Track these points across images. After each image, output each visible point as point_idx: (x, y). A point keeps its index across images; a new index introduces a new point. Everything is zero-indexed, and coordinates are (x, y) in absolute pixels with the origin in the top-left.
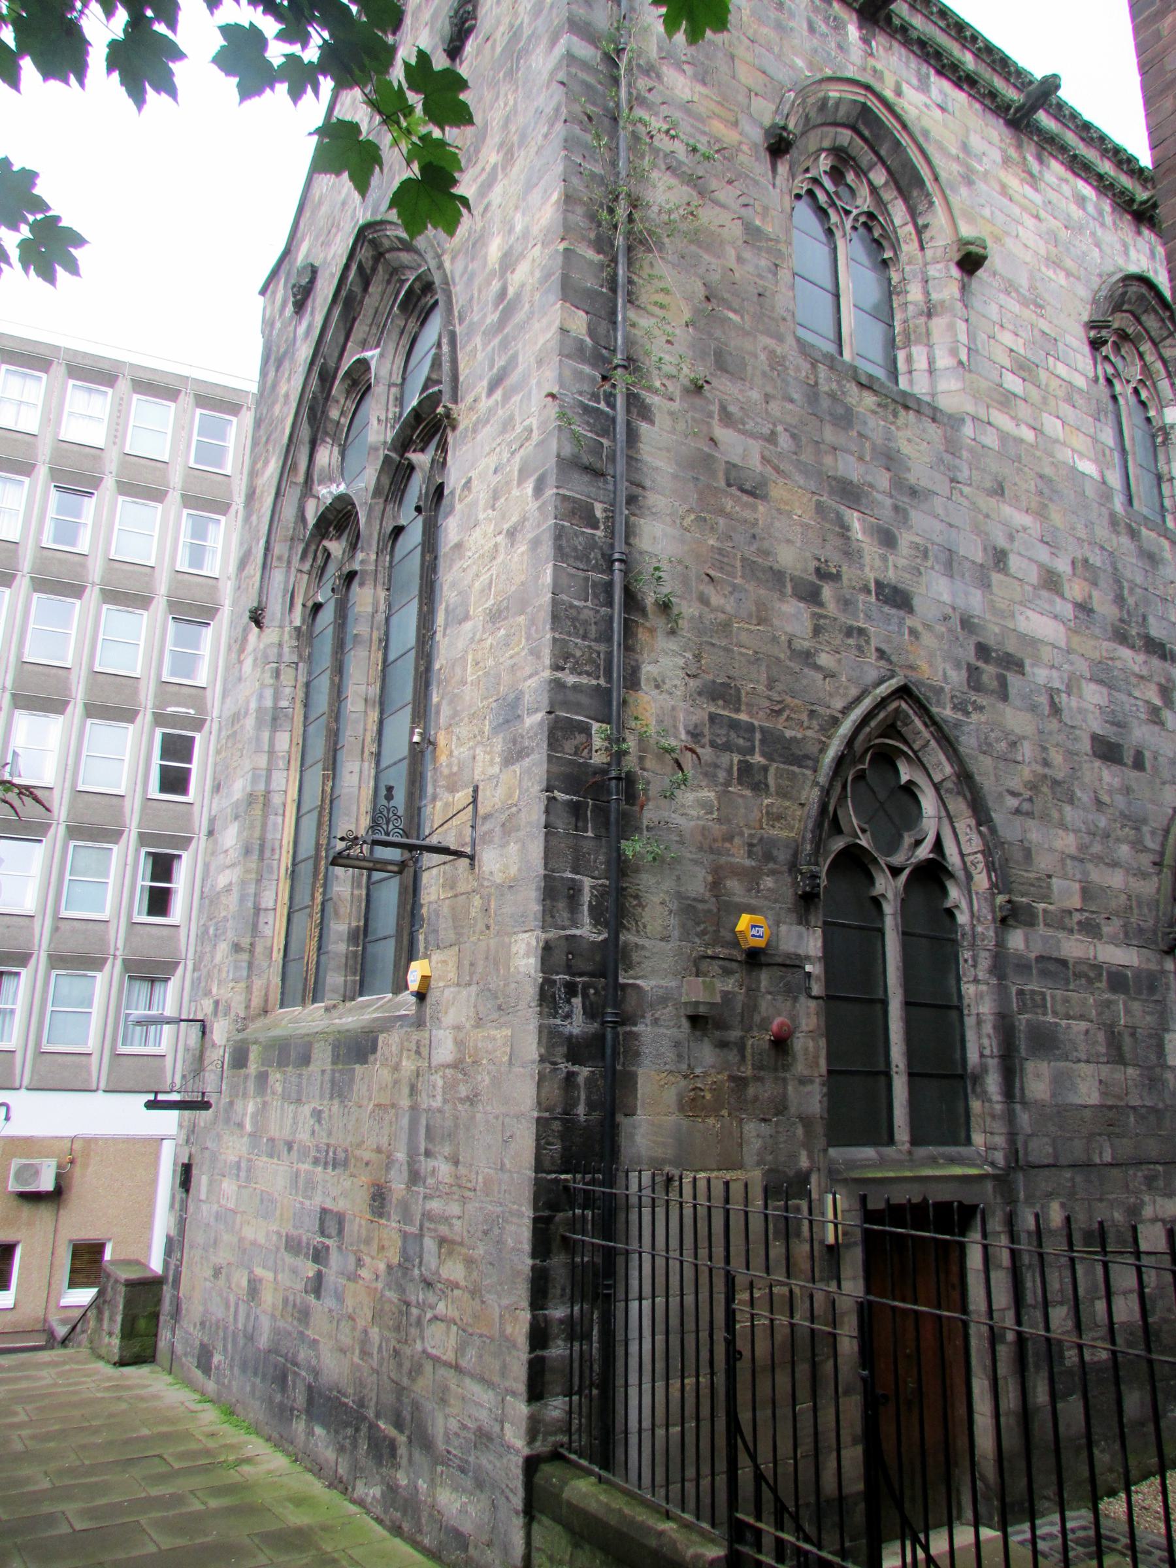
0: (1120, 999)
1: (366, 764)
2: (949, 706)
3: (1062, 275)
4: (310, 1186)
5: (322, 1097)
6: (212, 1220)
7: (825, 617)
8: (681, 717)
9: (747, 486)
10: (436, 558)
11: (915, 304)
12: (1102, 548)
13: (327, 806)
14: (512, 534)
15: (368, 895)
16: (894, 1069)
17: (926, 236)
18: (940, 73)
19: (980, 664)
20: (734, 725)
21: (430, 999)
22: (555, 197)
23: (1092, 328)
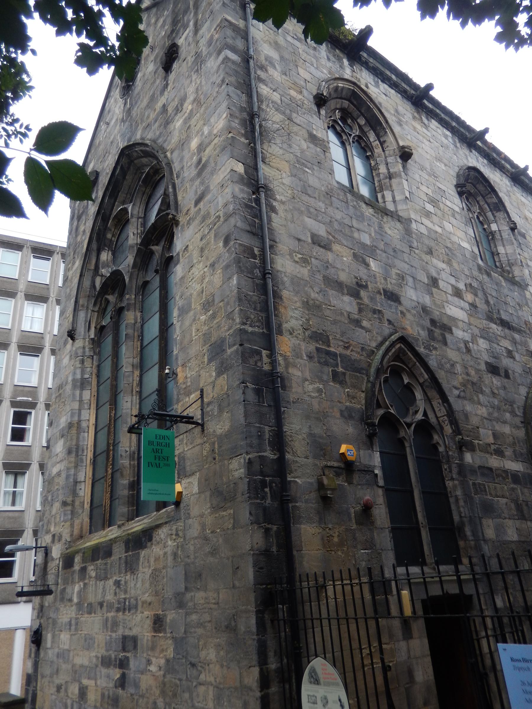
0: (518, 487)
1: (134, 397)
2: (422, 347)
3: (443, 165)
4: (115, 624)
5: (120, 573)
6: (55, 658)
7: (363, 304)
8: (303, 348)
9: (322, 244)
10: (167, 292)
12: (476, 279)
16: (421, 525)
17: (385, 145)
18: (383, 81)
19: (433, 328)
20: (328, 353)
21: (182, 505)
22: (225, 115)
23: (458, 187)
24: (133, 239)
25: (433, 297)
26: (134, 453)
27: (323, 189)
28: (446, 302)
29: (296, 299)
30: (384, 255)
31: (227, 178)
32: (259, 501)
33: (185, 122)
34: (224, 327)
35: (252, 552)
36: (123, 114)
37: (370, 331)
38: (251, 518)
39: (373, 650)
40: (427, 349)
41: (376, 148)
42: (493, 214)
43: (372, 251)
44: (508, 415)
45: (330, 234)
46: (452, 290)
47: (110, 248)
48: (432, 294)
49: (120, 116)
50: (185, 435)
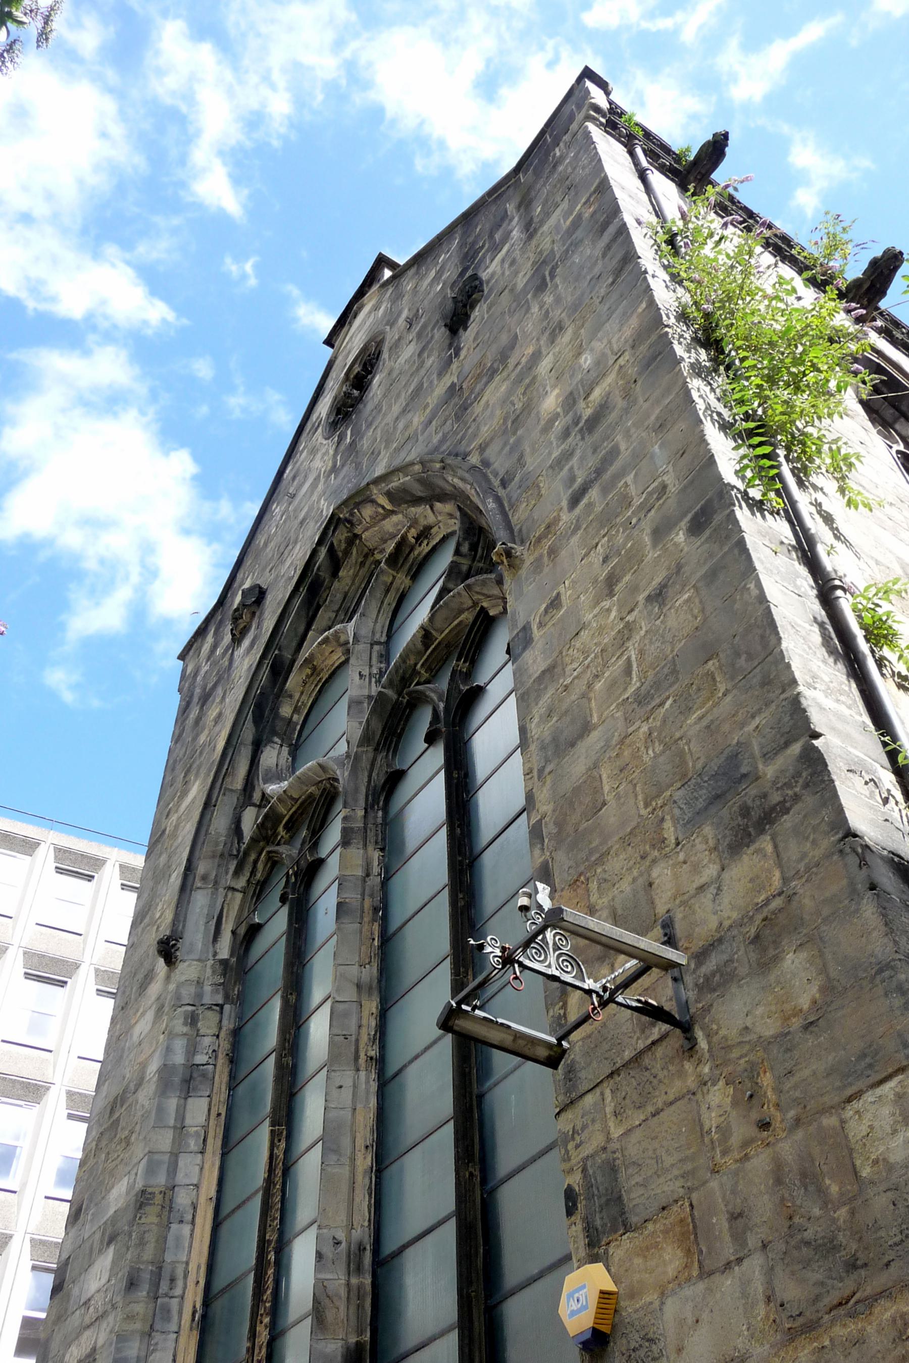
1: (363, 1074)
10: (466, 775)
13: (278, 1179)
15: (374, 1285)
24: (361, 687)
26: (361, 1249)
47: (285, 738)
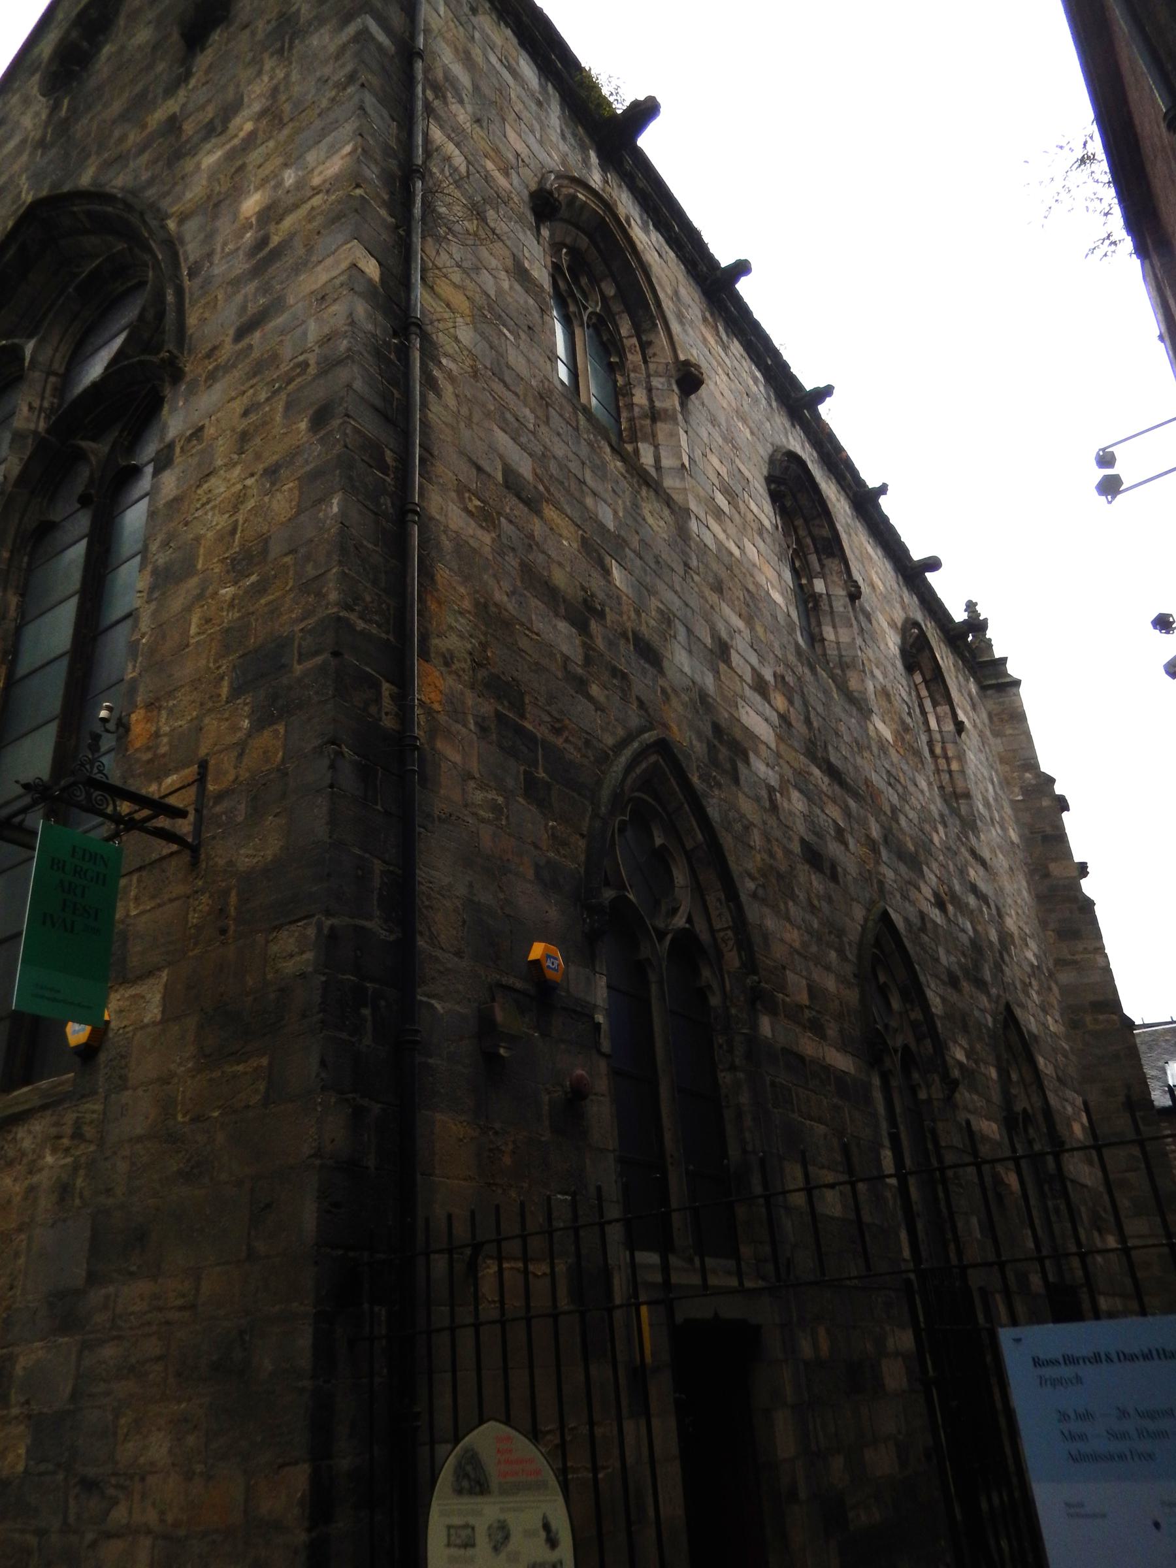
3: (748, 431)
7: (594, 650)
9: (524, 495)
11: (641, 406)
14: (272, 473)
17: (650, 351)
20: (520, 731)
22: (348, 149)
23: (773, 482)
24: (28, 420)
25: (720, 680)
27: (534, 383)
28: (741, 697)
29: (462, 590)
30: (638, 562)
31: (337, 282)
32: (344, 1036)
33: (230, 156)
34: (292, 611)
35: (318, 1162)
36: (46, 127)
37: (603, 710)
38: (323, 1075)
39: (568, 1438)
40: (704, 781)
41: (630, 351)
42: (820, 560)
43: (618, 544)
44: (833, 955)
45: (541, 481)
46: (753, 679)
48: (718, 672)
49: (36, 135)
50: (135, 878)
